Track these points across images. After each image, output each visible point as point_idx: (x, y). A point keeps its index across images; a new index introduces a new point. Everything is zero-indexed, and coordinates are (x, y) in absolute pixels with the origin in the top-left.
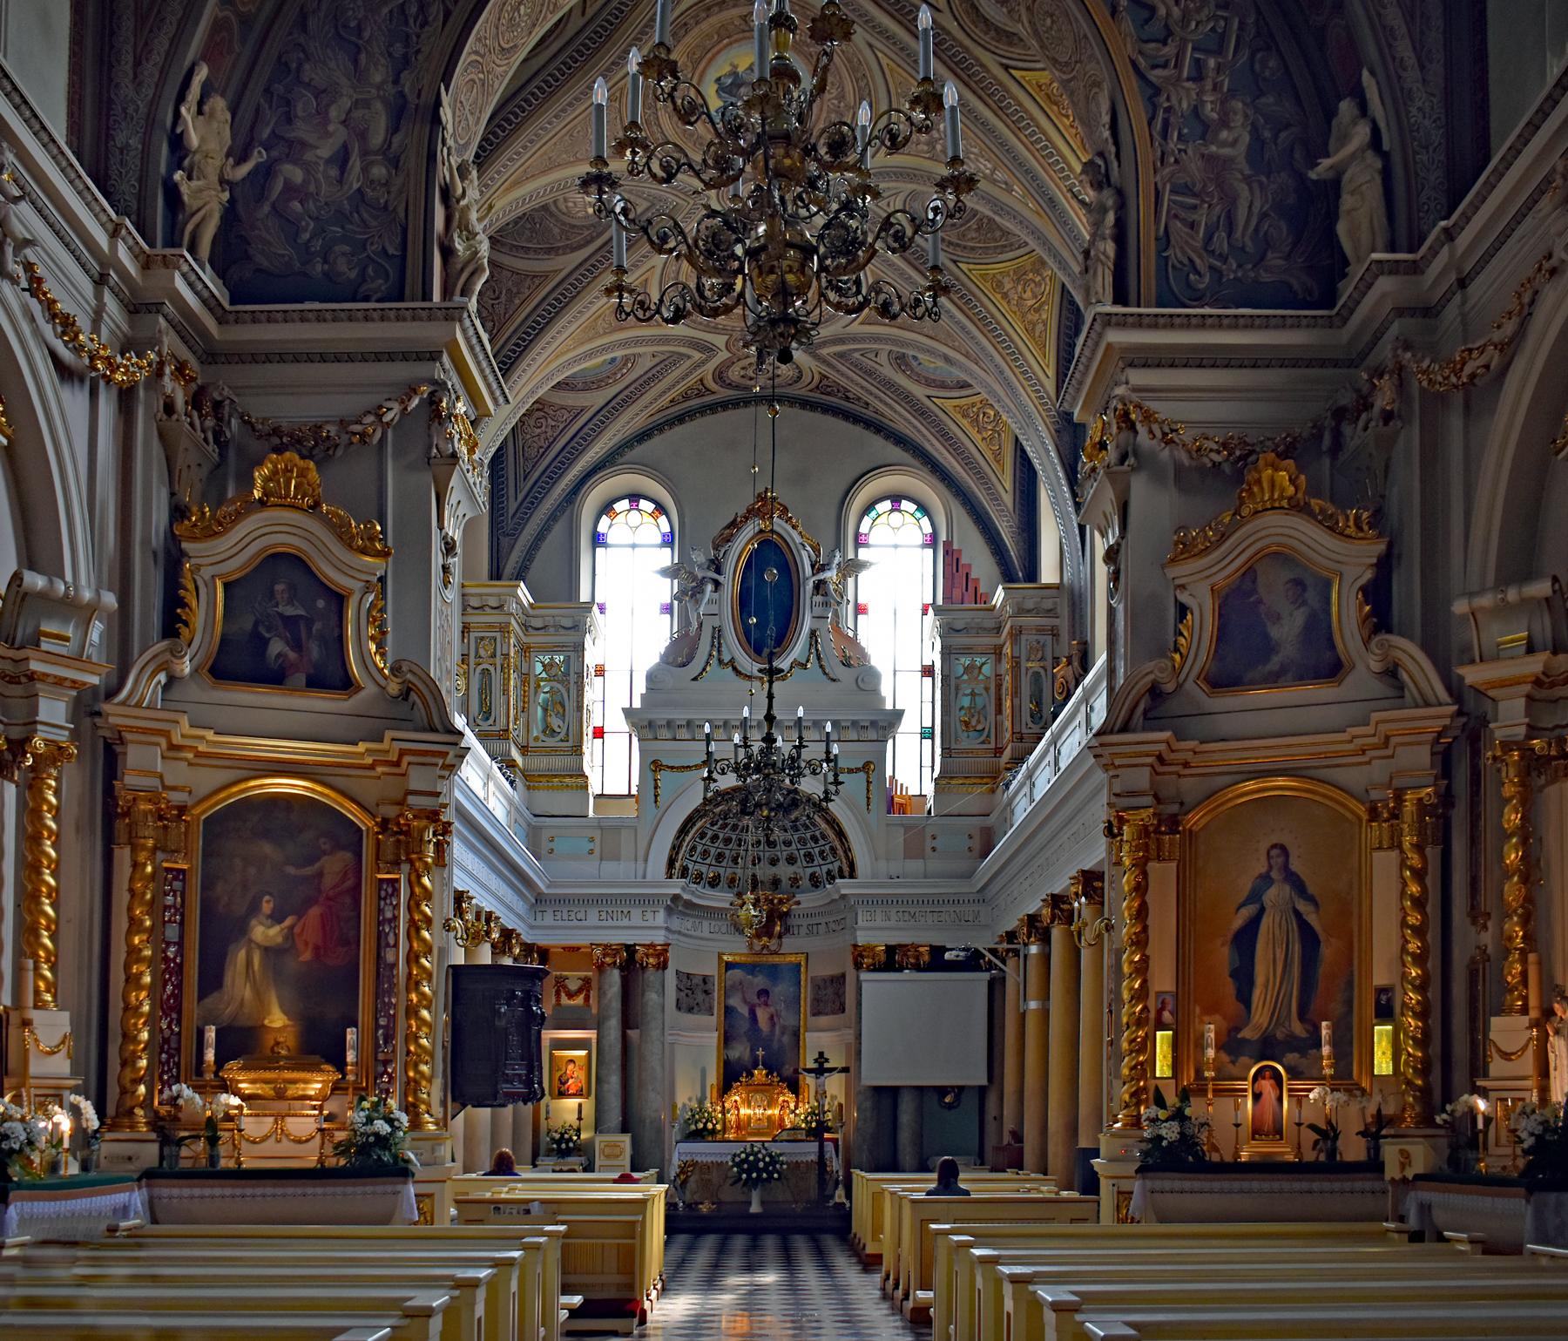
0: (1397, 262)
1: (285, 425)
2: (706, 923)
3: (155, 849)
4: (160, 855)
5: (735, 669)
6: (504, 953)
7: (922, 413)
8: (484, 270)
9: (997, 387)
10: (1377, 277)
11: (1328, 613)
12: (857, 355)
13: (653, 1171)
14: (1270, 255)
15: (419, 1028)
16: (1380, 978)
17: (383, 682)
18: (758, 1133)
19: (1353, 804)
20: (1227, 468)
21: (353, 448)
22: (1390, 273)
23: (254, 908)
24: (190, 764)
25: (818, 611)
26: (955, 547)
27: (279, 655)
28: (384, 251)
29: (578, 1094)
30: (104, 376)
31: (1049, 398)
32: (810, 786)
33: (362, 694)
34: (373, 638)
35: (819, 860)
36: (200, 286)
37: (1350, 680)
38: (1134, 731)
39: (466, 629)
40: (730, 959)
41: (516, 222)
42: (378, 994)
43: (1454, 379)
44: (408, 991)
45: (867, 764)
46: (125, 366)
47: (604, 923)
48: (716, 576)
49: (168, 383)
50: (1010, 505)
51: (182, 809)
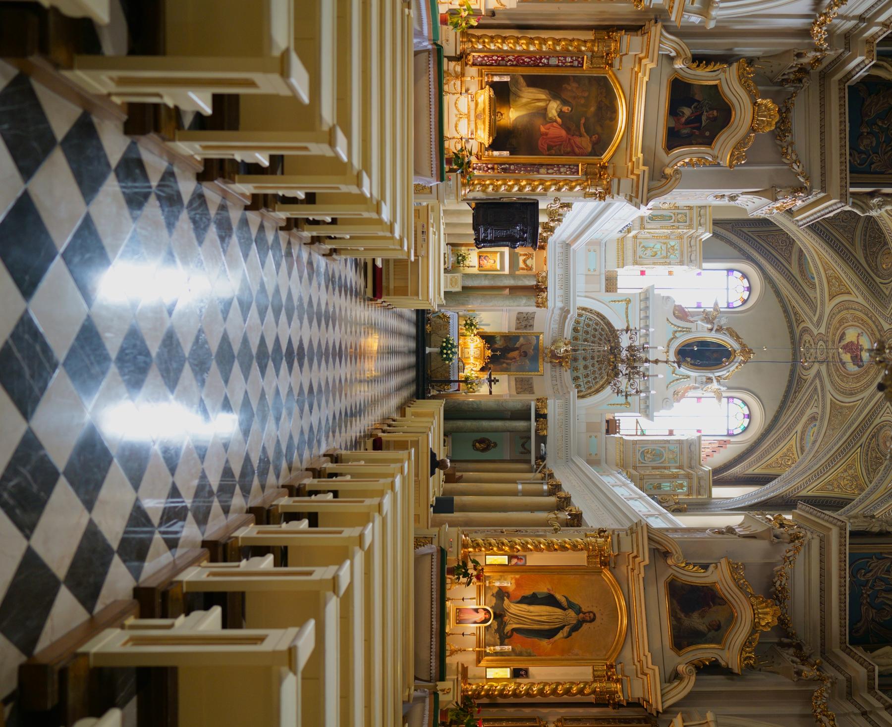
0: (874, 679)
1: (791, 114)
2: (557, 326)
3: (593, 51)
4: (590, 54)
5: (673, 339)
6: (544, 228)
7: (789, 429)
8: (863, 213)
9: (802, 467)
10: (866, 668)
11: (706, 642)
12: (816, 397)
13: (444, 302)
14: (874, 611)
15: (509, 186)
16: (533, 670)
17: (671, 165)
18: (462, 352)
19: (615, 656)
20: (773, 589)
21: (780, 148)
22: (868, 676)
23: (565, 102)
24: (632, 69)
25: (699, 379)
26: (728, 446)
27: (683, 113)
28: (873, 163)
29: (480, 266)
30: (817, 21)
31: (798, 493)
32: (623, 381)
33: (665, 155)
34: (691, 160)
35: (586, 380)
36: (857, 70)
37: (672, 653)
38: (649, 544)
39: (690, 208)
40: (541, 338)
41: (880, 230)
42: (525, 165)
43: (819, 710)
44: (527, 180)
45: (629, 404)
46: (821, 32)
47: (557, 277)
48: (715, 329)
49: (811, 55)
50: (747, 472)
51: (611, 65)
